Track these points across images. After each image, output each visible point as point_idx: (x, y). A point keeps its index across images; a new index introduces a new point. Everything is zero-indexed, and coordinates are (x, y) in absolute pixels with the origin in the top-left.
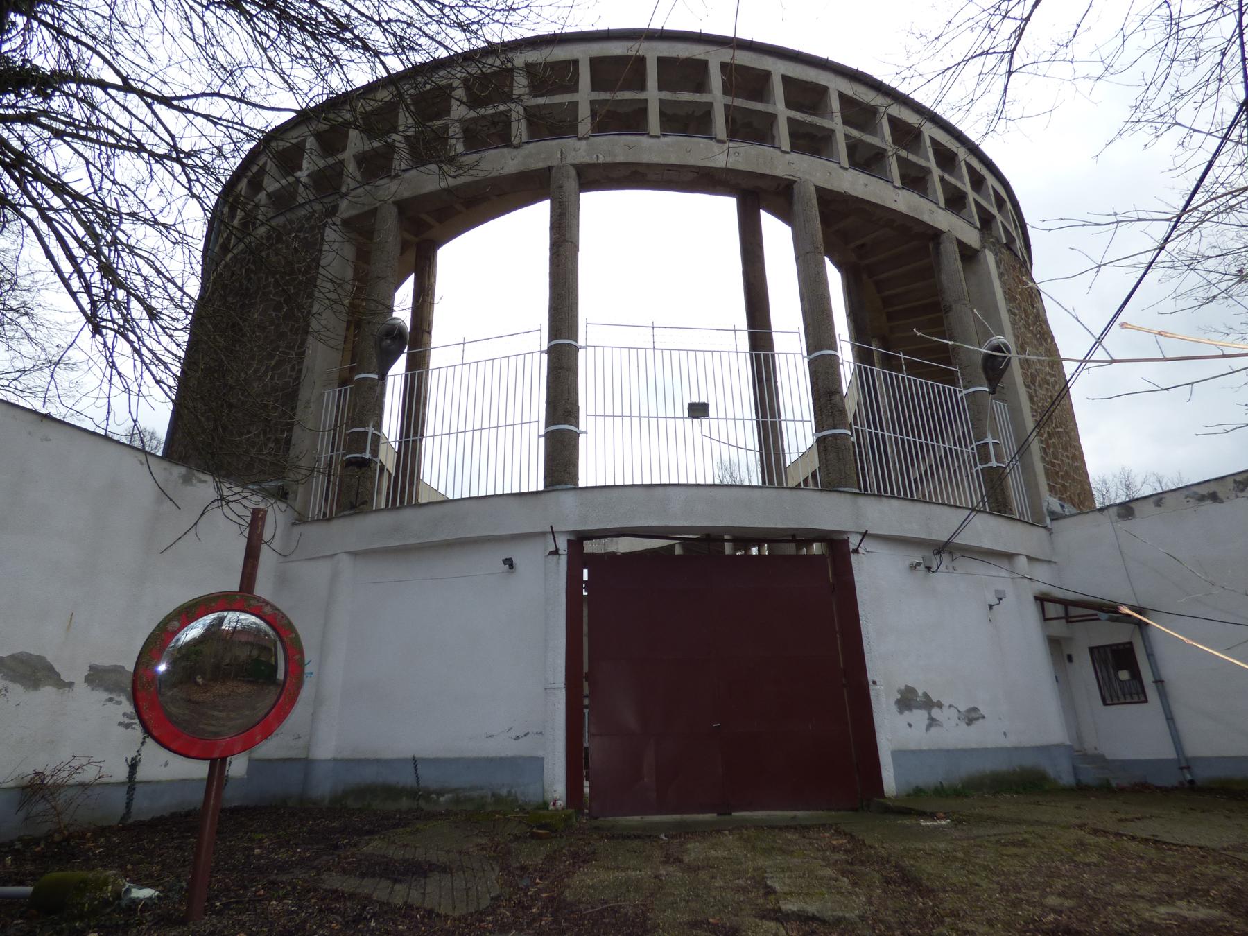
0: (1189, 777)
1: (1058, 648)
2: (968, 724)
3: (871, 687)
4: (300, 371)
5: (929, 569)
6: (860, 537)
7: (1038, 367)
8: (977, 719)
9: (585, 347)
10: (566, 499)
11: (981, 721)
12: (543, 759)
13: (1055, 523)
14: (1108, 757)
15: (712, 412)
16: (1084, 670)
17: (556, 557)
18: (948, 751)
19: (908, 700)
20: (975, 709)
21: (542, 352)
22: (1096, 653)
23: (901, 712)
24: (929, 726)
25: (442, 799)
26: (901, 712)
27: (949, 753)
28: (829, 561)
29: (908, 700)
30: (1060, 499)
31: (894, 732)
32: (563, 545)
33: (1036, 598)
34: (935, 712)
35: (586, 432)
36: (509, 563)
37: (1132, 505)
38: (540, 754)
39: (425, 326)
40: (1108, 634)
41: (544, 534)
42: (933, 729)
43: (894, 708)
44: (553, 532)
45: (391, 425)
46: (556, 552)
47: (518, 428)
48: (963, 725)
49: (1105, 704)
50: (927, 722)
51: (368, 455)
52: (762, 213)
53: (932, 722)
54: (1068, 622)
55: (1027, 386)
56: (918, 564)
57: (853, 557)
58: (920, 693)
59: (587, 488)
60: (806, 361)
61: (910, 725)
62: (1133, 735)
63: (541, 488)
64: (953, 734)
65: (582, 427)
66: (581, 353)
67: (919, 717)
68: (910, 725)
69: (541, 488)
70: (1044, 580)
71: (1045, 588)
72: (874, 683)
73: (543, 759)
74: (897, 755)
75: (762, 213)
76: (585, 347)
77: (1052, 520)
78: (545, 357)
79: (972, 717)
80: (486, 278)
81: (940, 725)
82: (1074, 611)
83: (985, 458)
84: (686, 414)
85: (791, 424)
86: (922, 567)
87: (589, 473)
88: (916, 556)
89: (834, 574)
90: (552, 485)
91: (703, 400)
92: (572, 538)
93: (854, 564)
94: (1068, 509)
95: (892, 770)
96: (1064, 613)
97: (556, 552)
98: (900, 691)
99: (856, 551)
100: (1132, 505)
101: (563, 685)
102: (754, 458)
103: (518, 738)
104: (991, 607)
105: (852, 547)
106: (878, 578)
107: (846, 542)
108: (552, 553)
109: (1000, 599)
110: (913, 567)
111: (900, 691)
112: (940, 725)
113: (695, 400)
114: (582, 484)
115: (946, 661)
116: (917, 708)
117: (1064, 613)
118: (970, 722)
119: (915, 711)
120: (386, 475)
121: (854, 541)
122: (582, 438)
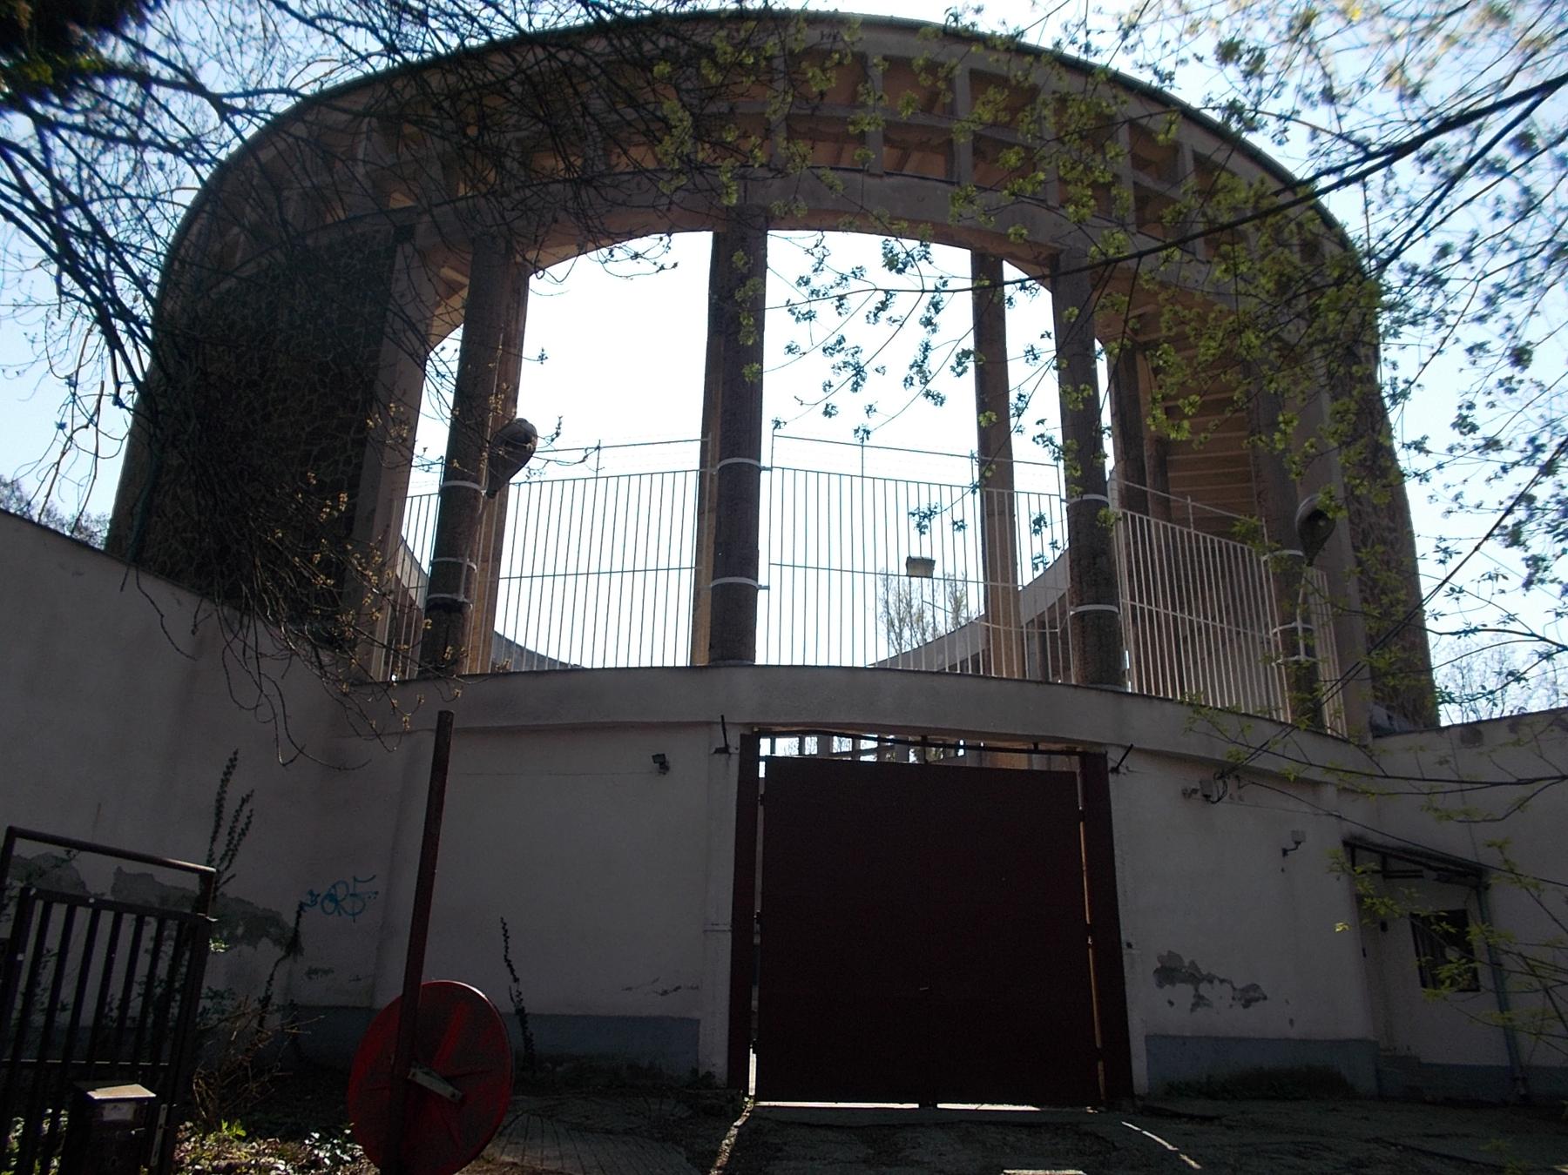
0: (1523, 1092)
1: (1372, 924)
3: (1125, 951)
4: (359, 467)
5: (1207, 797)
6: (1122, 753)
7: (1373, 519)
8: (1257, 1000)
9: (770, 469)
12: (698, 1021)
13: (1379, 741)
14: (1423, 1060)
15: (937, 572)
16: (1402, 939)
17: (724, 756)
18: (1217, 1039)
19: (1169, 972)
22: (1420, 925)
23: (1160, 985)
24: (1195, 1006)
25: (559, 1069)
26: (1160, 985)
28: (1079, 779)
29: (1169, 972)
30: (1388, 708)
31: (1151, 1009)
32: (734, 741)
33: (1346, 843)
34: (1204, 988)
35: (768, 588)
36: (662, 763)
37: (1481, 728)
38: (696, 1014)
39: (711, 519)
40: (1430, 899)
41: (709, 724)
44: (723, 724)
45: (419, 527)
46: (725, 750)
49: (1424, 985)
50: (1193, 1000)
51: (462, 598)
52: (1005, 263)
53: (1199, 1001)
54: (1385, 877)
55: (1356, 549)
56: (1195, 791)
57: (1112, 778)
58: (1186, 962)
60: (1064, 505)
61: (1171, 1003)
62: (1453, 1031)
64: (1225, 1017)
65: (762, 580)
66: (764, 475)
67: (1183, 993)
68: (1171, 1003)
70: (1357, 816)
71: (1357, 830)
72: (1129, 945)
73: (698, 1021)
74: (1155, 1040)
75: (1005, 263)
76: (770, 469)
77: (1375, 737)
79: (1250, 996)
80: (609, 334)
81: (1209, 1005)
82: (1395, 865)
83: (1292, 649)
84: (904, 571)
86: (1199, 795)
87: (776, 644)
88: (1193, 779)
89: (1085, 799)
90: (723, 658)
91: (926, 555)
92: (747, 732)
93: (1112, 786)
94: (1399, 722)
95: (1144, 1058)
96: (1381, 862)
97: (725, 750)
99: (1116, 770)
100: (1481, 728)
101: (728, 927)
103: (665, 993)
104: (1285, 852)
105: (1111, 765)
106: (1142, 805)
107: (1104, 757)
108: (718, 751)
109: (1298, 843)
110: (1187, 794)
111: (1160, 958)
112: (1209, 1005)
113: (915, 554)
115: (1223, 919)
116: (1183, 981)
117: (1381, 862)
118: (1247, 1004)
121: (1114, 756)
122: (762, 595)
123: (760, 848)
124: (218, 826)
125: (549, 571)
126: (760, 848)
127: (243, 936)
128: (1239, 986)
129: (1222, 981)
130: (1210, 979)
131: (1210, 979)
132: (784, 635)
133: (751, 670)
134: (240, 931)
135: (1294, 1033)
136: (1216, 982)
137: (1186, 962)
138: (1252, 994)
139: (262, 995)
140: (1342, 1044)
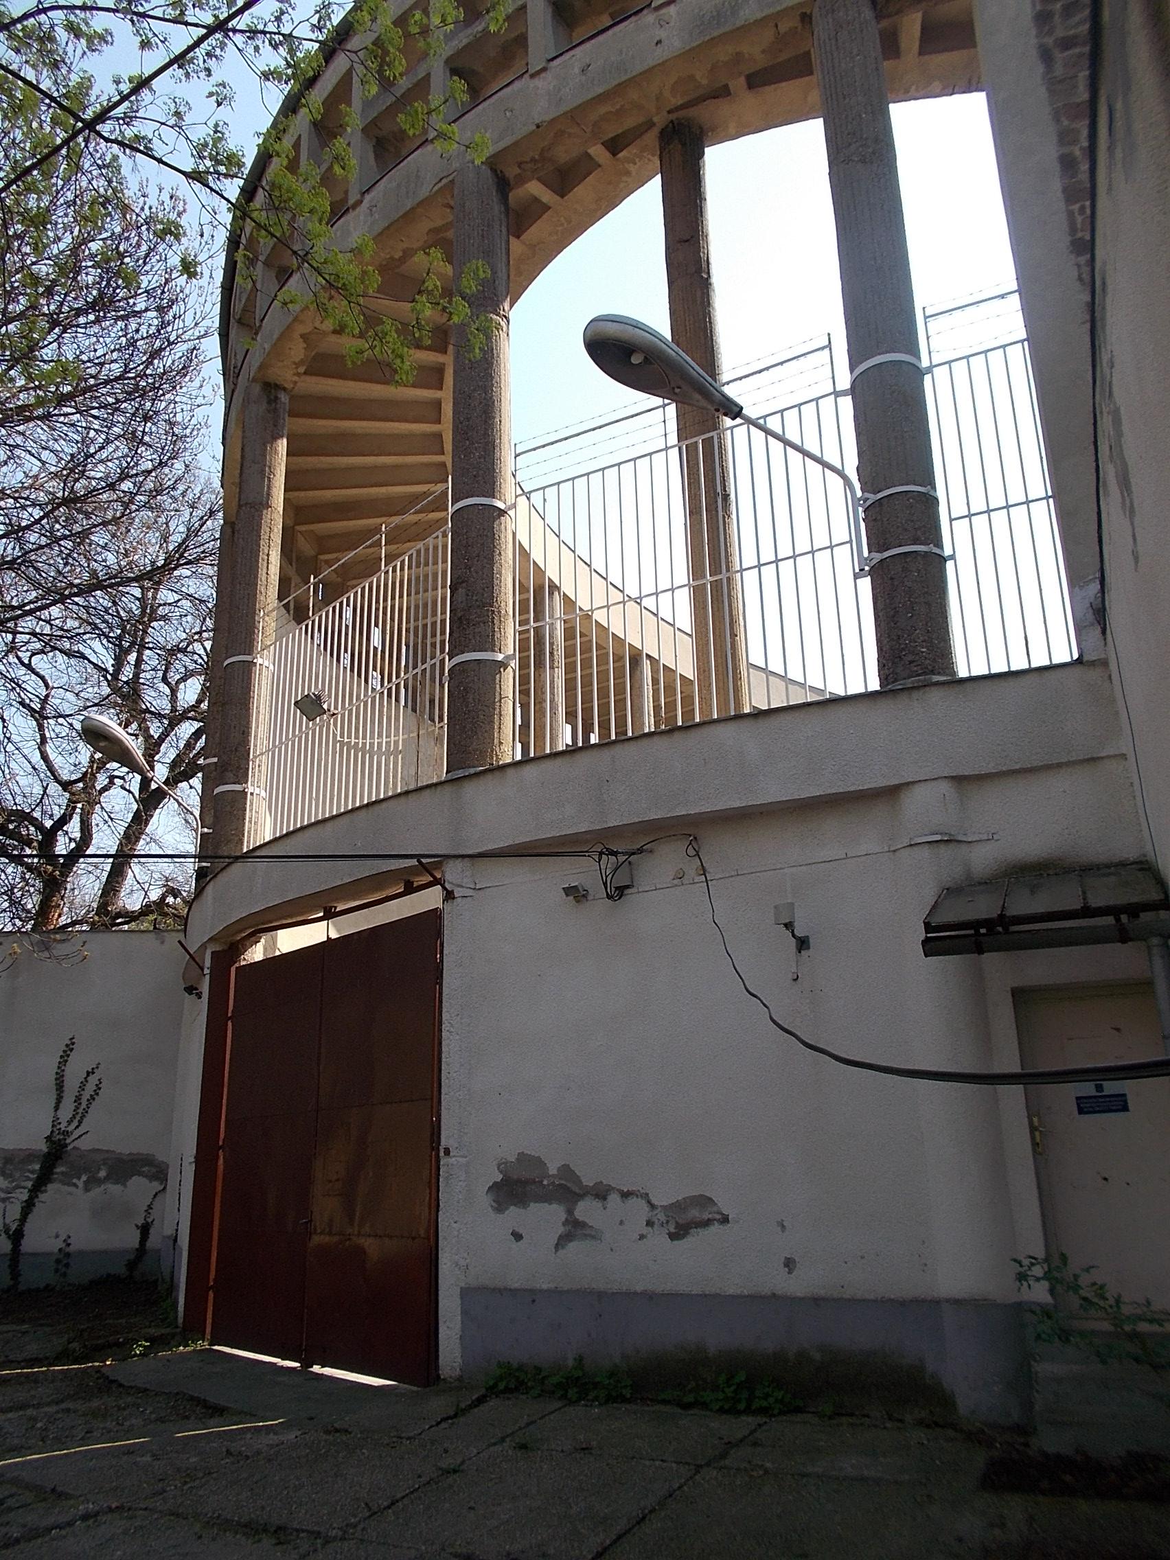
2: (673, 1237)
8: (707, 1223)
10: (926, 711)
11: (715, 1228)
18: (600, 1295)
19: (516, 1187)
20: (704, 1201)
21: (837, 394)
23: (500, 1208)
26: (500, 1208)
27: (602, 1302)
31: (477, 1245)
34: (586, 1210)
42: (572, 1246)
43: (484, 1201)
47: (804, 563)
48: (659, 1239)
53: (575, 1229)
58: (553, 1170)
59: (971, 679)
61: (518, 1236)
63: (874, 685)
64: (630, 1256)
67: (544, 1219)
68: (518, 1236)
69: (874, 685)
78: (847, 403)
79: (689, 1218)
81: (595, 1236)
85: (961, 527)
88: (584, 872)
98: (503, 1166)
102: (682, 611)
112: (595, 1236)
114: (963, 673)
119: (533, 1206)
120: (647, 666)
123: (226, 1075)
124: (59, 1100)
125: (785, 551)
126: (226, 1075)
127: (107, 1178)
128: (662, 1198)
129: (626, 1195)
130: (601, 1193)
131: (601, 1193)
132: (191, 849)
133: (489, 782)
134: (102, 1174)
135: (796, 1285)
136: (614, 1198)
137: (553, 1170)
138: (694, 1213)
139: (140, 1222)
140: (926, 1309)
